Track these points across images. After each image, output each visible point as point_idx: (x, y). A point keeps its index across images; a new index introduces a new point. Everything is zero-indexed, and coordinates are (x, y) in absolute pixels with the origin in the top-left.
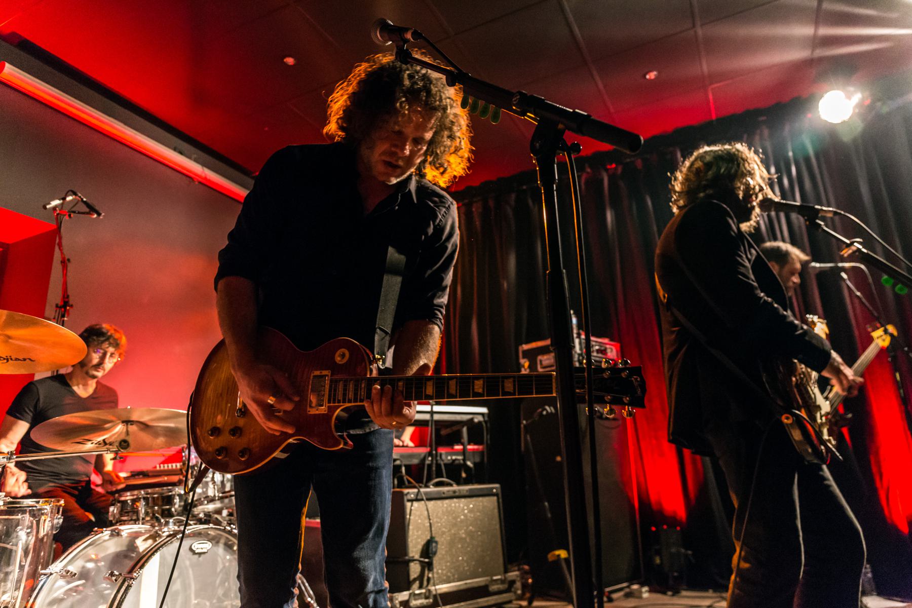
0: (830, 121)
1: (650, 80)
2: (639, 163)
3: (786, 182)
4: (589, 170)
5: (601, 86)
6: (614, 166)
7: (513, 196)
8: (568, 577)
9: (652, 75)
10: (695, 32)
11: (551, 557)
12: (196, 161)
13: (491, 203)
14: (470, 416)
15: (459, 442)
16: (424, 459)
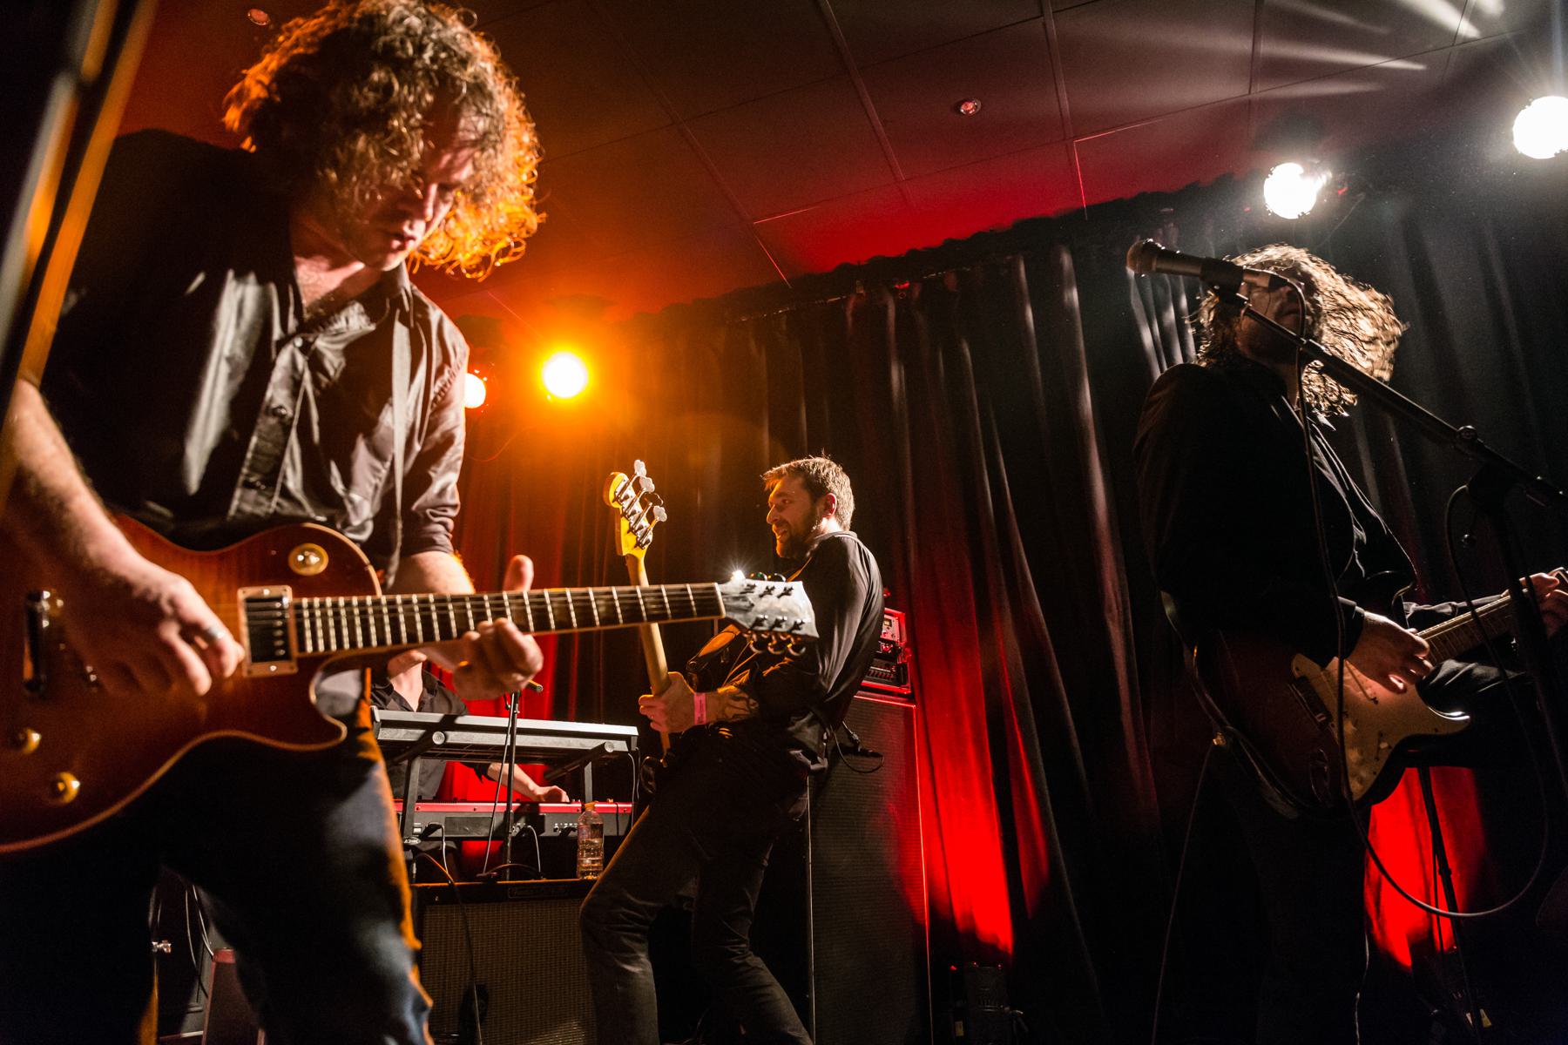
2: (951, 280)
10: (1044, 25)
14: (601, 742)
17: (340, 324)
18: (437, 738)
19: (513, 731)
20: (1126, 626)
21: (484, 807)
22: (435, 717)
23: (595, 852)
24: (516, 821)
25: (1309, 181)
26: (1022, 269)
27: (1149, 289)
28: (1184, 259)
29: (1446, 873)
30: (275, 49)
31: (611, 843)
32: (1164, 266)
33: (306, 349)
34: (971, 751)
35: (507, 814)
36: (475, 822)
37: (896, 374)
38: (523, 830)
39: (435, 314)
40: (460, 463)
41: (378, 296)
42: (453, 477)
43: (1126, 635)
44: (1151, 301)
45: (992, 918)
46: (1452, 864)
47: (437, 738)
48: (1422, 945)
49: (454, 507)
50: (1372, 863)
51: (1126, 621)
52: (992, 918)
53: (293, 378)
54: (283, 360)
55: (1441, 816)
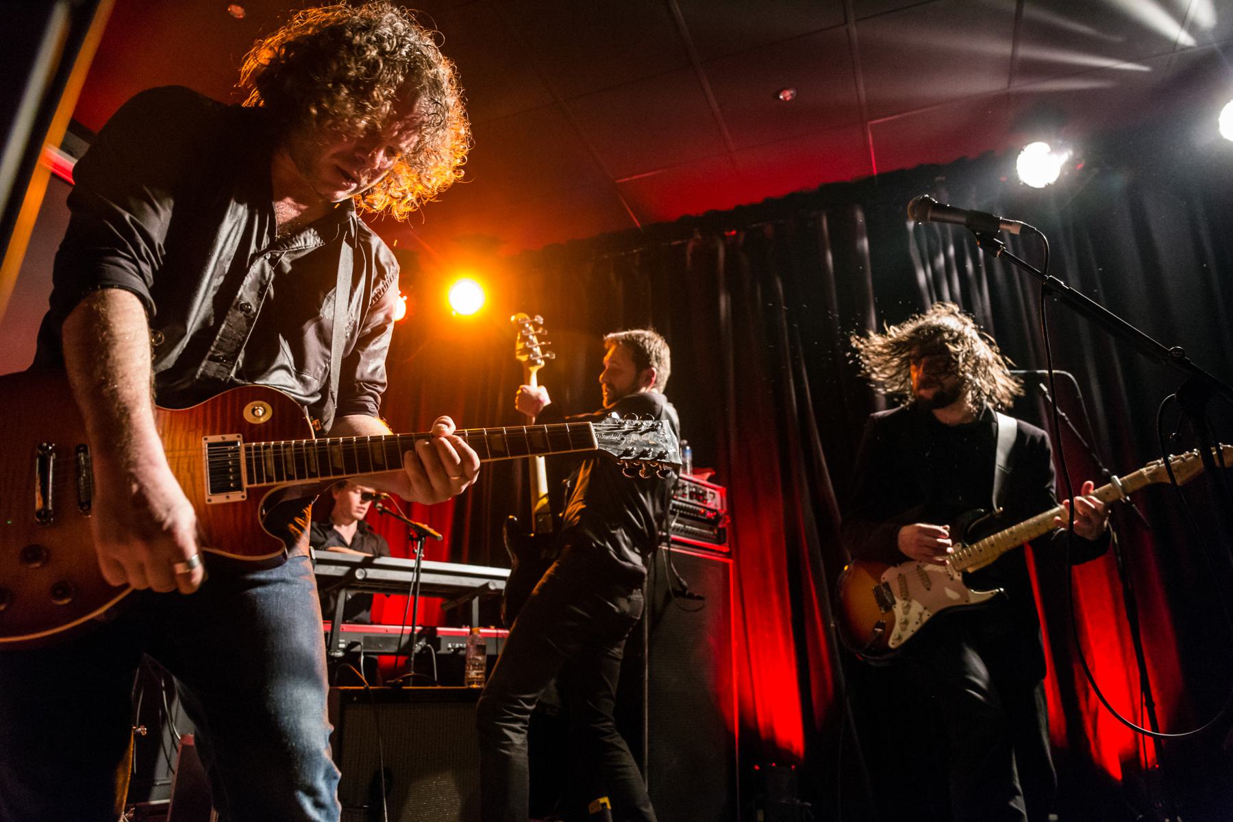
0: (1031, 184)
3: (970, 266)
4: (699, 237)
5: (715, 105)
6: (734, 232)
8: (272, 491)
9: (786, 95)
10: (848, 31)
11: (593, 809)
15: (468, 623)
16: (410, 644)
17: (300, 244)
18: (359, 574)
19: (418, 570)
21: (395, 629)
22: (358, 556)
23: (480, 666)
24: (418, 640)
25: (1055, 156)
26: (825, 222)
27: (924, 240)
28: (952, 210)
29: (1150, 704)
31: (491, 660)
32: (936, 215)
33: (274, 261)
34: (775, 597)
35: (412, 634)
36: (387, 640)
37: (723, 302)
38: (424, 648)
39: (375, 241)
40: (386, 352)
41: (331, 223)
42: (381, 362)
44: (926, 250)
45: (789, 730)
46: (1156, 698)
47: (359, 574)
48: (1131, 763)
49: (382, 385)
50: (1093, 694)
52: (789, 730)
53: (261, 283)
54: (255, 269)
55: (1147, 660)
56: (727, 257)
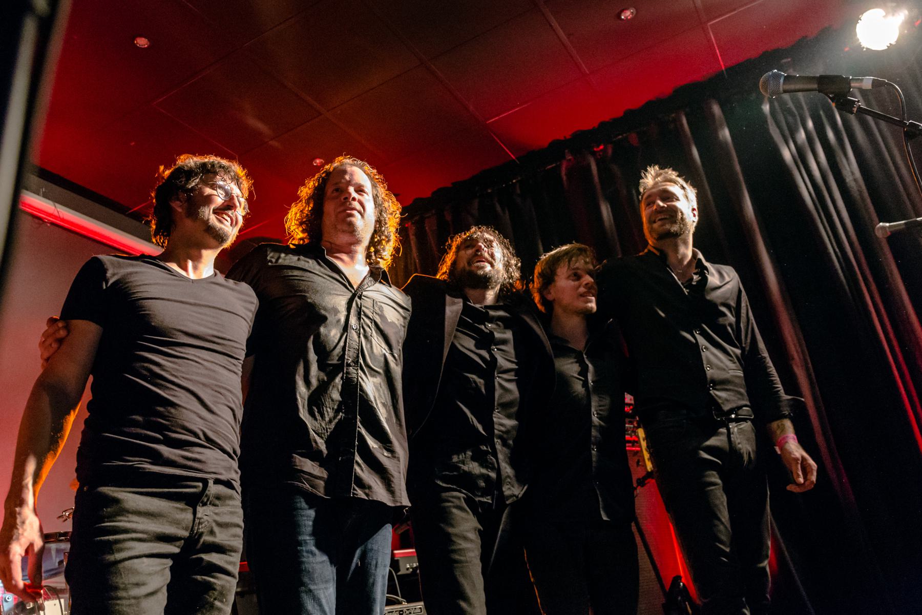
1: (627, 20)
2: (633, 138)
3: (831, 135)
6: (602, 147)
7: (476, 203)
9: (627, 15)
12: (45, 196)
13: (448, 217)
20: (807, 369)
25: (890, 18)
26: (684, 121)
27: (781, 118)
30: (587, 284)
37: (605, 211)
43: (809, 376)
44: (785, 128)
51: (807, 364)
56: (599, 170)
